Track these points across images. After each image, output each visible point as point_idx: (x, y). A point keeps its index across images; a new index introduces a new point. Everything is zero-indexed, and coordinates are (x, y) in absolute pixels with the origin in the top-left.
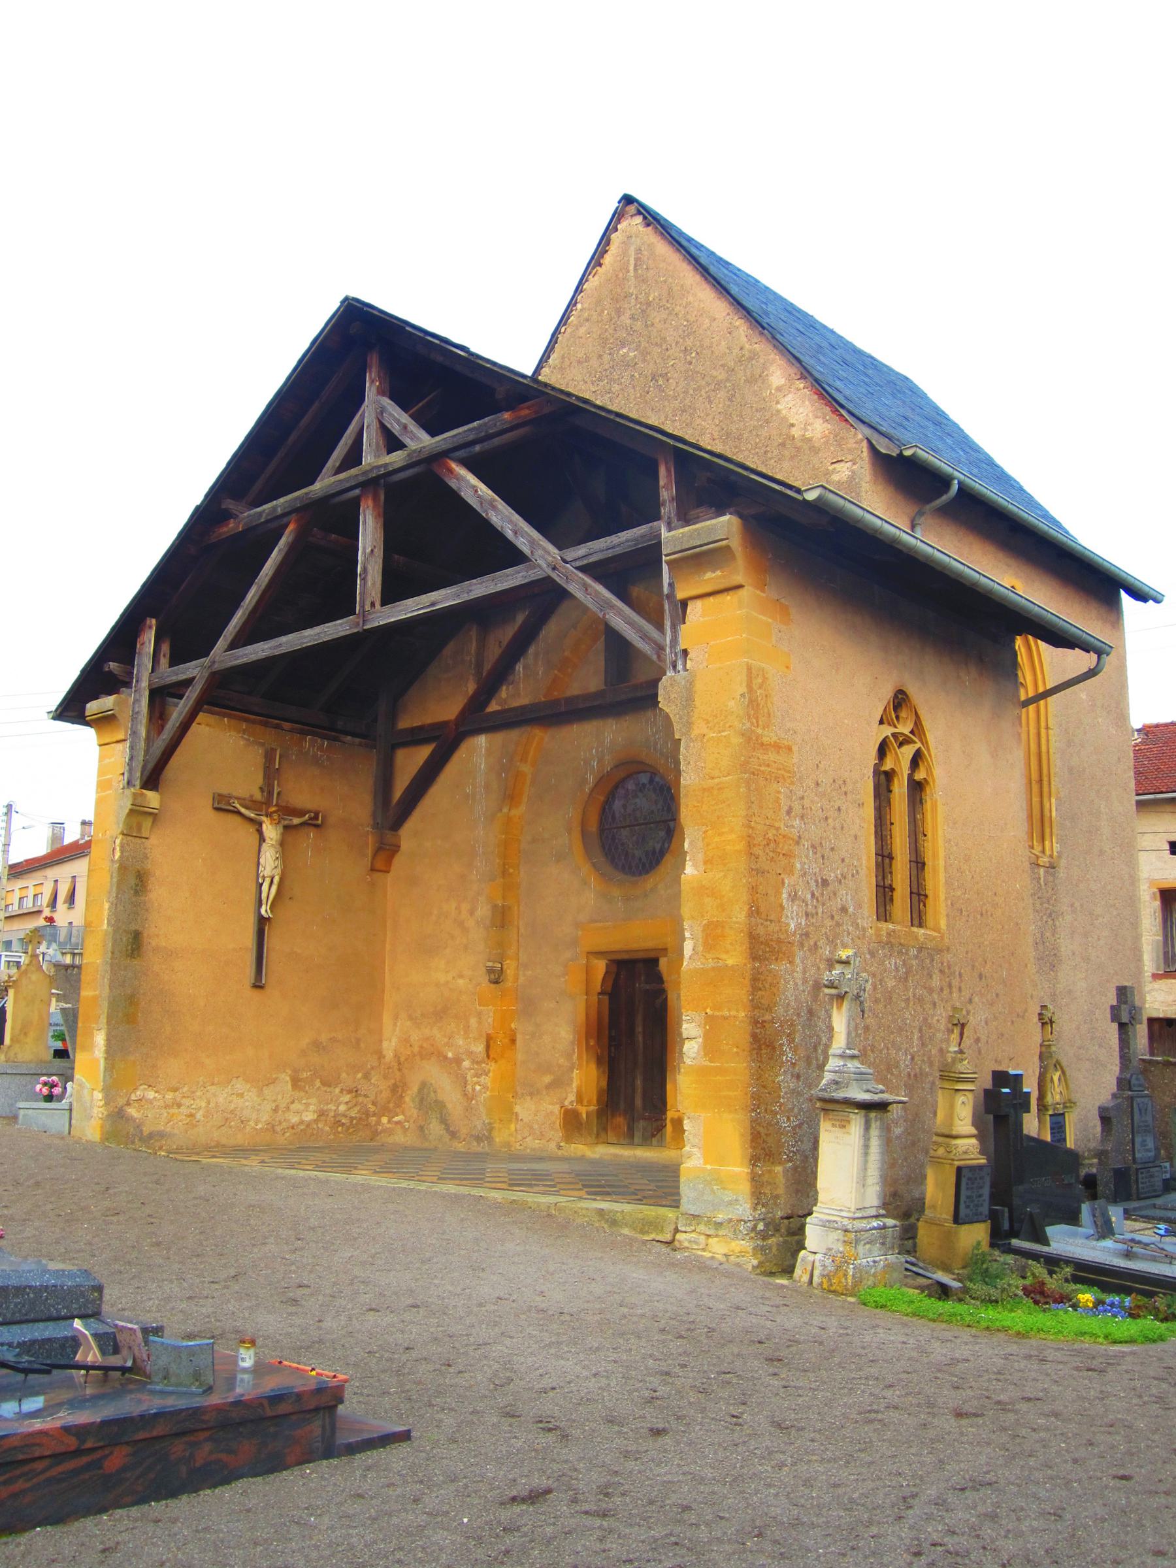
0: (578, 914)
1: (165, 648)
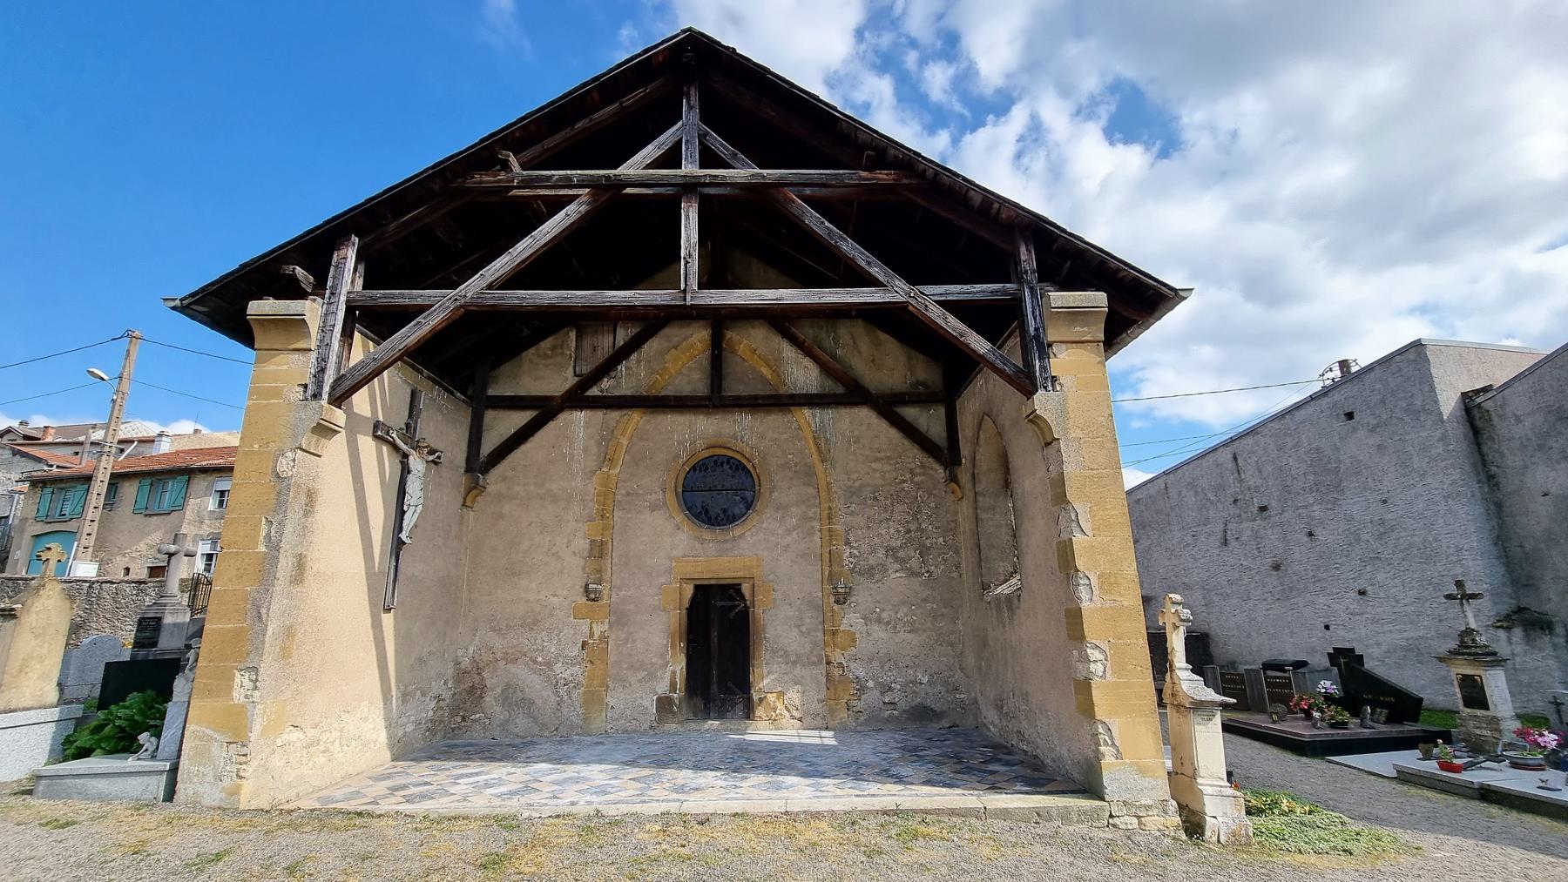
0: (670, 553)
1: (361, 269)
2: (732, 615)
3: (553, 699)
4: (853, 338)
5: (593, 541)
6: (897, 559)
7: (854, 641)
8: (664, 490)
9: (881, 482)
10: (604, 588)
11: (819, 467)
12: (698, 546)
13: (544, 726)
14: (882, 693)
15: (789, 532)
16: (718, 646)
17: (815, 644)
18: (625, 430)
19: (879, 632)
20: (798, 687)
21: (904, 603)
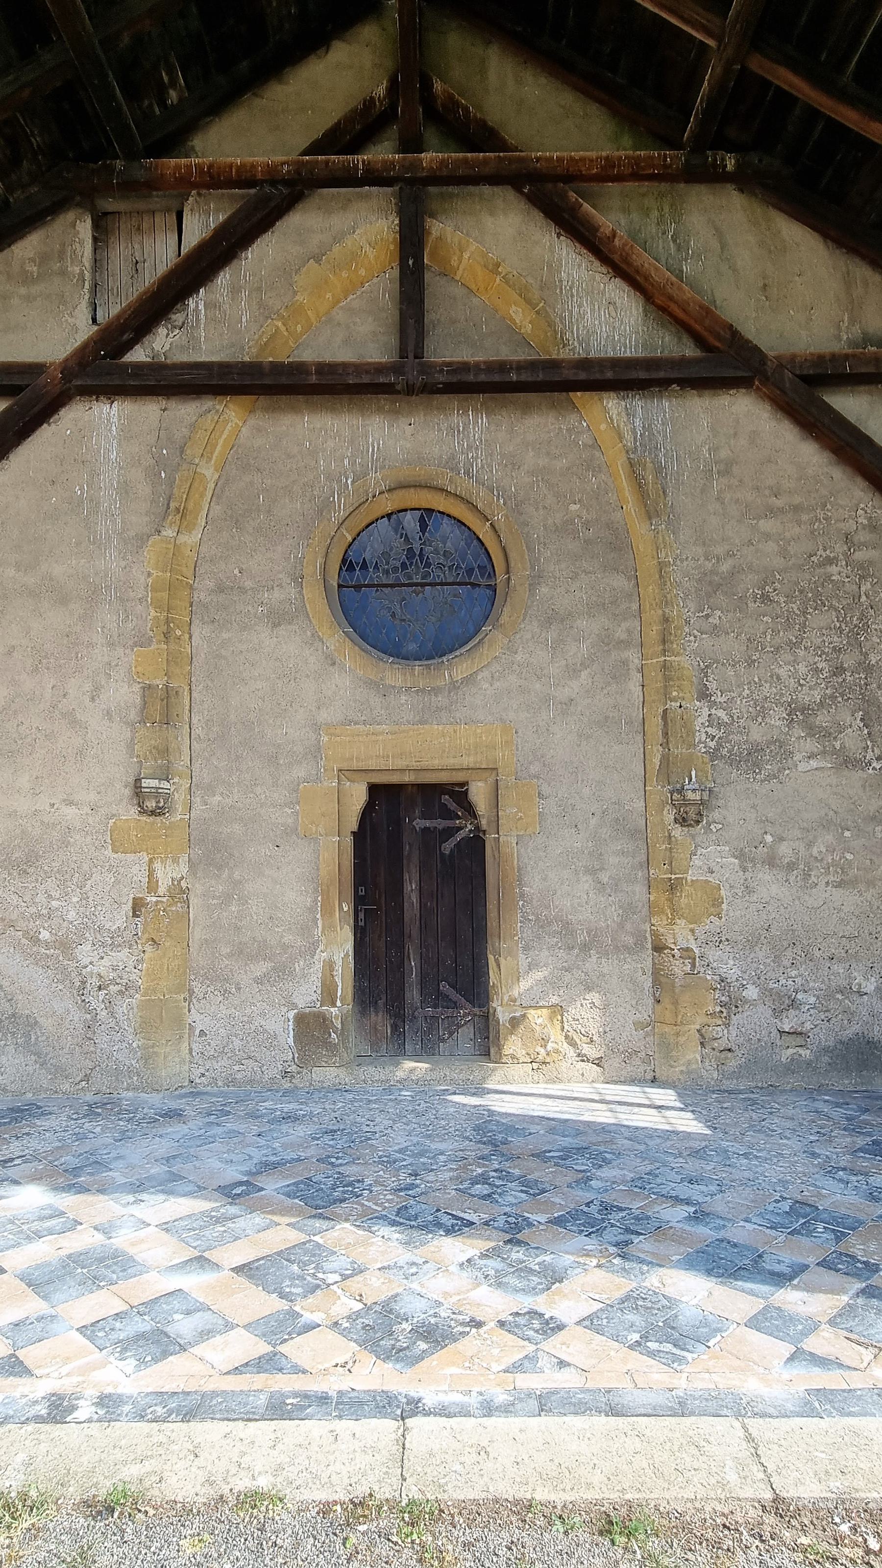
2: (448, 847)
3: (77, 1016)
4: (719, 233)
5: (147, 689)
6: (812, 730)
7: (717, 902)
8: (299, 580)
9: (778, 562)
10: (177, 789)
11: (641, 531)
12: (376, 701)
13: (59, 1071)
14: (777, 1013)
15: (573, 672)
16: (421, 900)
17: (629, 909)
18: (209, 446)
19: (770, 886)
20: (595, 997)
21: (826, 824)
